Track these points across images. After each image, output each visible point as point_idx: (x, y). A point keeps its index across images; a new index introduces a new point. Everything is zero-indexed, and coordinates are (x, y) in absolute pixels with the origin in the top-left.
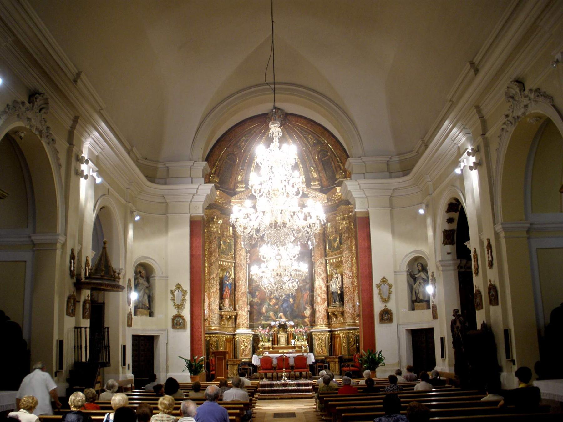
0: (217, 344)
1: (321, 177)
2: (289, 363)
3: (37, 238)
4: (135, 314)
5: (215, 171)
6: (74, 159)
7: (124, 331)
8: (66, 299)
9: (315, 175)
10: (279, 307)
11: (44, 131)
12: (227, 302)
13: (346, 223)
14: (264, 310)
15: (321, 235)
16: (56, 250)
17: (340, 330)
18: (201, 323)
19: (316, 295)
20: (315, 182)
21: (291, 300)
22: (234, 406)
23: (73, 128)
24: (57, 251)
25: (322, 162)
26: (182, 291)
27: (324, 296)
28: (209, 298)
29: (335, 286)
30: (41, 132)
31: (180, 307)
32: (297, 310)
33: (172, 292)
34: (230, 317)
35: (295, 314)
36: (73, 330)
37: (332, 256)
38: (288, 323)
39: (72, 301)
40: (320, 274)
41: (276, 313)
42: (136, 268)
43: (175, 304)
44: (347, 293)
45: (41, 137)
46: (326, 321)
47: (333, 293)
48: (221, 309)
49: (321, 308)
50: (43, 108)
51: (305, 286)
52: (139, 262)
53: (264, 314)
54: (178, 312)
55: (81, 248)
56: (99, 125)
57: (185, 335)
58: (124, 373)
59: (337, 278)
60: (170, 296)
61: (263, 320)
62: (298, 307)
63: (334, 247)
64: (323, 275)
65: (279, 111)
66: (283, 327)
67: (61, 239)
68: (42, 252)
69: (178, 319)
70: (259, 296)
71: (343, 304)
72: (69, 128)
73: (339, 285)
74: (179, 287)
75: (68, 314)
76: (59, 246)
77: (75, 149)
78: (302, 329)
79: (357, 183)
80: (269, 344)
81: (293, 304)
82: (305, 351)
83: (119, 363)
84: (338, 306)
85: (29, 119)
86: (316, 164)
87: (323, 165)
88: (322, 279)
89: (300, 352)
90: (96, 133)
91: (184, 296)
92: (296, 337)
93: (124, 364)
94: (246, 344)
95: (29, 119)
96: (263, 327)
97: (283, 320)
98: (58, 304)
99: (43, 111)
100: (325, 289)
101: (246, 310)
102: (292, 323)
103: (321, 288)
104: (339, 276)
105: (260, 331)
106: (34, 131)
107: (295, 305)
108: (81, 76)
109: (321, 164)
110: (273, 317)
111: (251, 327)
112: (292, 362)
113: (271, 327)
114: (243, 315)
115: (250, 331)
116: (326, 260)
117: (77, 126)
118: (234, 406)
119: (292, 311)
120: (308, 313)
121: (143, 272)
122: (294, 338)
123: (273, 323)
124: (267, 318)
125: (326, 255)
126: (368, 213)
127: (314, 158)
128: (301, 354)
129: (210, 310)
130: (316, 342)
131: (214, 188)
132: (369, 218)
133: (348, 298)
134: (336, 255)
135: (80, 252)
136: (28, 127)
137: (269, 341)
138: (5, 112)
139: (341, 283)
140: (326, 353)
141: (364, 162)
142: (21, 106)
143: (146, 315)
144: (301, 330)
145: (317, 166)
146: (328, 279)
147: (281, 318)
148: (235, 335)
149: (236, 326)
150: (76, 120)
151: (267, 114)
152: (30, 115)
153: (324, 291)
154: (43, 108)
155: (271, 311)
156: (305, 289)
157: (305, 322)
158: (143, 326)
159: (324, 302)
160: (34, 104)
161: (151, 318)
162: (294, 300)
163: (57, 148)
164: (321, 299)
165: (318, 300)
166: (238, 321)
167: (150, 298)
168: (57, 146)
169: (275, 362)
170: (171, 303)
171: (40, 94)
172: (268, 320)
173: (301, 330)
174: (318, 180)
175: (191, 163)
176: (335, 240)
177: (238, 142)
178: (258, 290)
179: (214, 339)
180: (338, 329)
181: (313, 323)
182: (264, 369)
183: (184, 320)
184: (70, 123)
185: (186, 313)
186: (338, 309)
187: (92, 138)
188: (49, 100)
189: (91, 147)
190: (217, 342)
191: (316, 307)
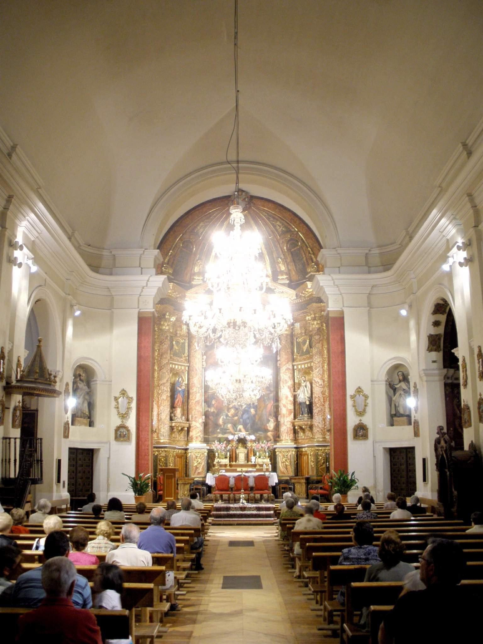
0: (166, 460)
2: (248, 484)
9: (283, 268)
12: (178, 411)
13: (317, 324)
14: (221, 421)
15: (289, 337)
18: (148, 435)
20: (282, 275)
21: (252, 411)
27: (291, 407)
28: (158, 407)
29: (303, 396)
31: (124, 416)
32: (259, 423)
33: (116, 399)
34: (182, 429)
35: (256, 427)
36: (1, 440)
38: (249, 438)
41: (235, 425)
43: (119, 413)
46: (292, 436)
47: (300, 404)
48: (171, 419)
49: (286, 421)
51: (269, 394)
52: (78, 364)
53: (221, 426)
54: (122, 422)
56: (36, 205)
57: (130, 449)
59: (306, 386)
60: (114, 403)
61: (219, 433)
63: (303, 351)
64: (290, 383)
66: (242, 441)
69: (122, 430)
73: (308, 395)
74: (123, 393)
78: (264, 445)
80: (226, 461)
81: (254, 416)
82: (267, 470)
84: (306, 419)
86: (284, 255)
88: (289, 387)
89: (261, 470)
90: (32, 215)
92: (258, 454)
93: (59, 481)
94: (200, 460)
96: (220, 440)
97: (243, 434)
100: (292, 399)
102: (253, 437)
103: (287, 397)
105: (216, 446)
107: (257, 417)
108: (17, 149)
109: (290, 256)
110: (231, 430)
111: (206, 441)
112: (251, 483)
113: (229, 441)
116: (293, 366)
119: (254, 423)
121: (83, 375)
122: (255, 455)
123: (231, 437)
124: (225, 431)
125: (293, 360)
126: (342, 312)
128: (263, 473)
129: (159, 420)
131: (167, 281)
134: (304, 359)
135: (11, 351)
137: (226, 458)
139: (310, 392)
140: (291, 473)
141: (339, 254)
143: (86, 425)
146: (295, 387)
147: (240, 431)
149: (188, 439)
150: (9, 199)
153: (290, 401)
155: (228, 423)
157: (268, 437)
158: (81, 437)
159: (290, 414)
162: (256, 411)
164: (287, 410)
166: (191, 434)
167: (91, 406)
170: (114, 412)
172: (225, 433)
173: (263, 445)
174: (286, 274)
176: (304, 342)
178: (215, 399)
179: (163, 454)
180: (306, 445)
181: (277, 438)
186: (306, 423)
187: (28, 221)
190: (166, 457)
191: (281, 419)
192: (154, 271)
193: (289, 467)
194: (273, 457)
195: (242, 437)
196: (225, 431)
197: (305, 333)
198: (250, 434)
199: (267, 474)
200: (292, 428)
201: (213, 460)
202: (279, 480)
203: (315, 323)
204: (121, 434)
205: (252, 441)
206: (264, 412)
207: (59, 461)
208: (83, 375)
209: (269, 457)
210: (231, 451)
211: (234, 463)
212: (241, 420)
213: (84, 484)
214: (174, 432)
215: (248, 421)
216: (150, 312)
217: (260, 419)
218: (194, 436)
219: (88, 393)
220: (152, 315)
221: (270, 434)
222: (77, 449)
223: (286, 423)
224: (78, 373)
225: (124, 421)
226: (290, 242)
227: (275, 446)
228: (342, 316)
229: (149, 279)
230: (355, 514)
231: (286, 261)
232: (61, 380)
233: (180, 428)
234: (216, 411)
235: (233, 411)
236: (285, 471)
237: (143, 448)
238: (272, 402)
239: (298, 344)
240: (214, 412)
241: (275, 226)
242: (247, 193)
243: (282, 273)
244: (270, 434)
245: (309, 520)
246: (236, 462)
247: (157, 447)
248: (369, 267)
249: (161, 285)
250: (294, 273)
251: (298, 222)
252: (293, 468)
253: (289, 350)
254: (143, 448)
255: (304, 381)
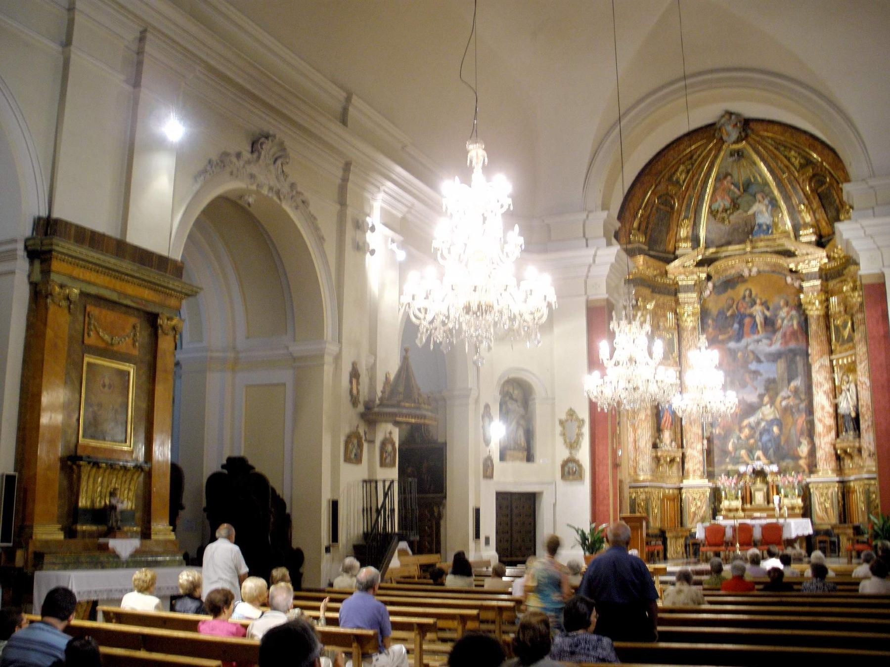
0: (647, 504)
1: (817, 221)
2: (752, 536)
3: (298, 349)
4: (502, 458)
5: (640, 225)
6: (349, 226)
7: (478, 486)
8: (342, 439)
9: (808, 218)
10: (756, 441)
11: (285, 189)
12: (667, 435)
13: (859, 296)
14: (730, 447)
15: (821, 319)
16: (323, 365)
17: (856, 480)
18: (607, 470)
19: (816, 421)
20: (806, 228)
21: (775, 429)
22: (877, 601)
23: (345, 180)
24: (326, 367)
25: (819, 195)
26: (577, 419)
27: (830, 422)
28: (635, 431)
29: (846, 405)
30: (278, 193)
31: (573, 445)
32: (786, 447)
33: (562, 423)
34: (672, 460)
35: (781, 453)
36: (361, 484)
37: (840, 352)
38: (767, 469)
39: (355, 441)
40: (821, 385)
41: (750, 451)
42: (504, 385)
43: (565, 442)
44: (863, 417)
45: (280, 199)
46: (833, 464)
47: (843, 416)
48: (655, 446)
49: (825, 441)
50: (280, 157)
51: (798, 404)
52: (506, 378)
53: (730, 453)
54: (571, 453)
55: (375, 360)
56: (393, 171)
57: (583, 490)
58: (477, 549)
59: (849, 390)
60: (559, 429)
61: (729, 463)
62: (787, 441)
63: (843, 337)
64: (827, 386)
65: (733, 117)
66: (760, 474)
67: (331, 348)
68: (305, 369)
69: (570, 465)
70: (722, 425)
71: (859, 435)
72: (338, 181)
73: (852, 403)
74: (571, 413)
75: (347, 459)
76: (328, 359)
77: (350, 211)
78: (792, 478)
79: (858, 226)
80: (737, 504)
81: (779, 437)
82: (781, 516)
83: (468, 534)
84: (851, 438)
85: (252, 176)
86: (807, 199)
87: (820, 198)
88: (825, 392)
89: (773, 516)
90: (389, 184)
91: (580, 427)
92: (782, 491)
93: (477, 536)
94: (699, 504)
95: (252, 176)
96: (728, 474)
97: (758, 465)
98: (329, 447)
99: (279, 162)
100: (831, 410)
101: (699, 447)
102: (774, 468)
103: (823, 408)
104: (853, 386)
105: (723, 482)
106: (265, 191)
107: (783, 439)
108: (353, 101)
109: (817, 198)
110: (746, 458)
111: (710, 476)
112: (757, 534)
113: (741, 476)
114: (694, 457)
115: (705, 482)
116: (831, 361)
117: (351, 177)
118: (877, 601)
119: (778, 448)
120: (804, 450)
121: (516, 393)
122: (778, 493)
123: (742, 469)
125: (831, 352)
126: (882, 276)
127: (803, 190)
128: (774, 521)
129: (636, 449)
130: (816, 500)
131: (624, 256)
132: (884, 284)
133: (867, 424)
134: (846, 350)
135: (372, 369)
136: (254, 187)
137: (737, 498)
138: (205, 171)
139: (855, 398)
140: (834, 519)
141: (872, 187)
142: (234, 160)
143: (521, 460)
144: (791, 479)
145: (810, 203)
146: (835, 392)
147: (759, 459)
148: (680, 489)
149: (683, 473)
150: (347, 167)
151: (712, 125)
152: (254, 169)
153: (828, 413)
154: (280, 157)
155: (742, 448)
156: (799, 410)
157: (800, 467)
158: (514, 477)
159: (829, 431)
160: (260, 154)
161: (529, 465)
162: (781, 429)
163: (312, 212)
164: (824, 426)
165: (819, 428)
166: (686, 466)
167: (529, 434)
168: (312, 209)
169: (729, 533)
170: (559, 440)
171: (267, 137)
173: (791, 479)
174: (812, 226)
175: (584, 216)
176: (845, 326)
177: (674, 173)
179: (643, 496)
181: (812, 468)
182: (710, 545)
183: (580, 466)
184: (340, 173)
185: (584, 455)
186: (852, 444)
187: (385, 192)
188: (286, 143)
189: (385, 206)
190: (647, 500)
191: (817, 441)
192: (604, 241)
193: (830, 511)
194: (806, 494)
195: (759, 468)
196: (737, 461)
197: (845, 310)
198: (772, 463)
199: (781, 521)
200: (833, 452)
201: (720, 502)
202: (814, 531)
203: (856, 294)
204: (570, 470)
205: (772, 473)
206: (793, 431)
207: (477, 512)
208: (516, 393)
209: (799, 496)
210: (744, 488)
211: (748, 506)
212: (760, 444)
213: (523, 541)
214: (662, 465)
215: (769, 445)
216: (604, 300)
217: (787, 441)
218: (691, 470)
219: (523, 417)
220: (604, 303)
221: (802, 462)
222: (511, 494)
223: (823, 446)
224: (506, 389)
225: (573, 452)
226: (814, 181)
227: (808, 480)
228: (881, 281)
229: (595, 255)
230: (800, 583)
231: (812, 208)
232: (477, 401)
233: (668, 459)
234: (722, 433)
235: (747, 431)
236: (825, 517)
237: (600, 488)
238: (804, 416)
239: (837, 328)
240: (720, 434)
241: (789, 159)
242: (738, 115)
243: (806, 226)
244: (802, 462)
245: (680, 592)
246: (751, 503)
247: (634, 487)
248: (873, 208)
249: (613, 260)
250: (824, 224)
251: (819, 147)
252: (836, 512)
253: (824, 338)
254: (601, 487)
255: (848, 382)
